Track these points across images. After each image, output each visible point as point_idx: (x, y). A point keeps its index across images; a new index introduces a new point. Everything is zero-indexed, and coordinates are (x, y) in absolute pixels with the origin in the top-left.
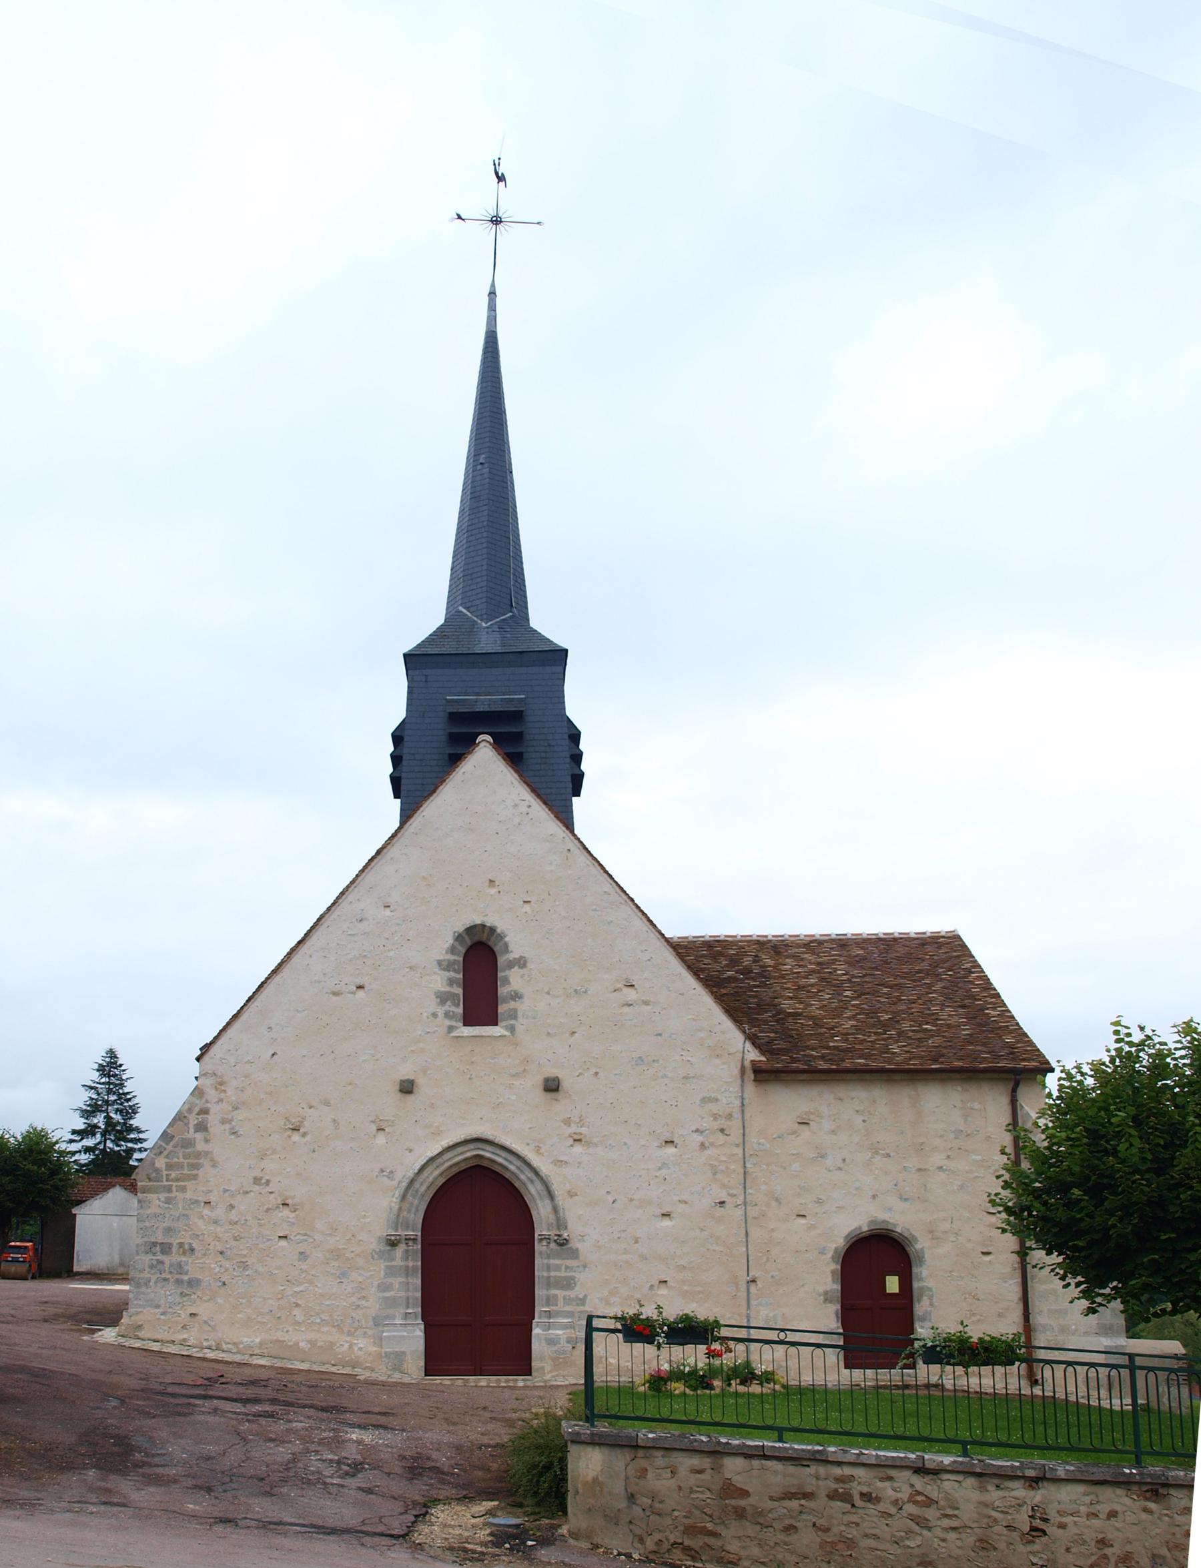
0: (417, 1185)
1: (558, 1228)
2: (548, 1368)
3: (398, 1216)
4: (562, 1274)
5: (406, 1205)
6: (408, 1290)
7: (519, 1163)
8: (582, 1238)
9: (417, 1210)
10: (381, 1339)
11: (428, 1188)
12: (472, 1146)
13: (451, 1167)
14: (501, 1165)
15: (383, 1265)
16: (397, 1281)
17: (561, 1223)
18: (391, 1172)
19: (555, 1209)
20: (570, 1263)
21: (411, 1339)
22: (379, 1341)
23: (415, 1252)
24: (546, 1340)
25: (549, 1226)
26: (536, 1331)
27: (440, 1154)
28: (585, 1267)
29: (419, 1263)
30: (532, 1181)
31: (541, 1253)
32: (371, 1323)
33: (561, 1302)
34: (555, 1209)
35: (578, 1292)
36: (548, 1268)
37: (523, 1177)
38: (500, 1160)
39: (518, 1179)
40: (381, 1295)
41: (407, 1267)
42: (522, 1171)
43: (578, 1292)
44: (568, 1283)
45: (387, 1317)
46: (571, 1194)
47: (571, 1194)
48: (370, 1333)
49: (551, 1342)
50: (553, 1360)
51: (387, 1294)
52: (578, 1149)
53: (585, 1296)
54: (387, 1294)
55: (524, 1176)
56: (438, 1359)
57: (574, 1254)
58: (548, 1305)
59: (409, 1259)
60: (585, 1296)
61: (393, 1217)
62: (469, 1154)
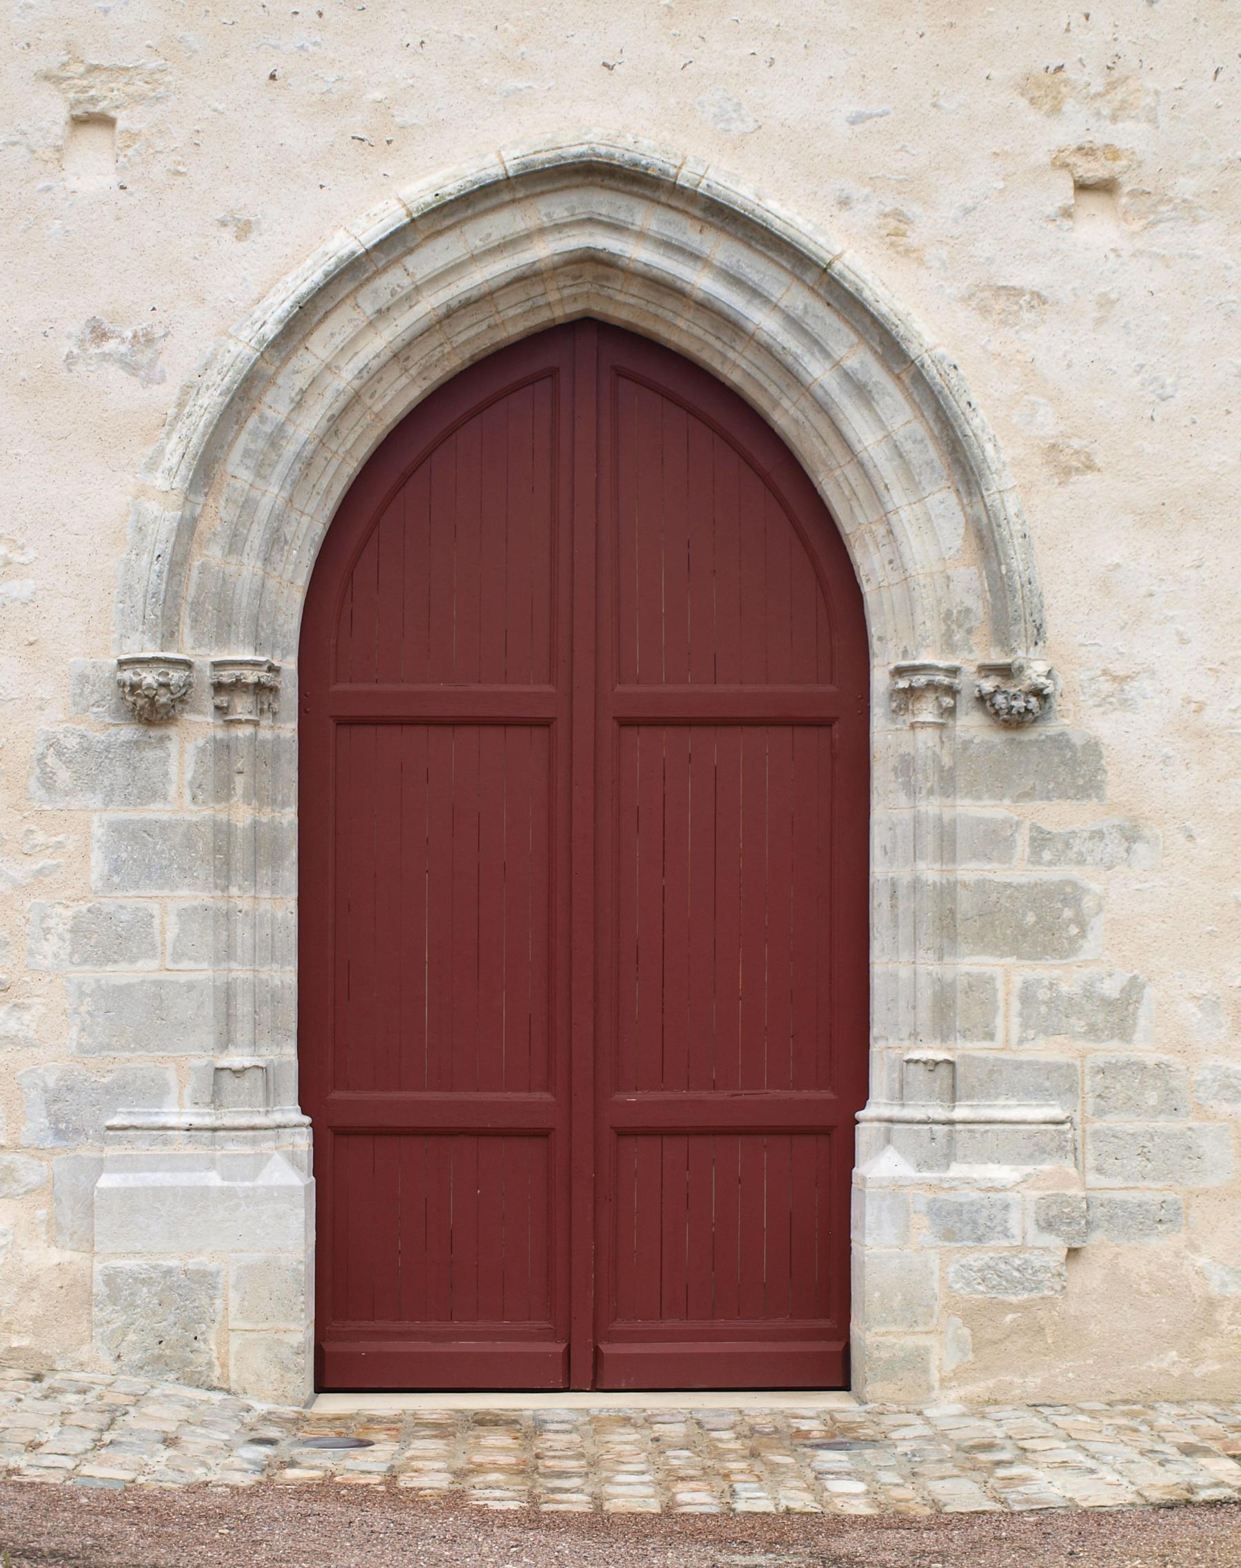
0: (275, 405)
1: (1002, 634)
2: (944, 1355)
3: (177, 565)
4: (1018, 871)
5: (218, 513)
6: (228, 953)
7: (796, 298)
8: (1119, 686)
9: (276, 541)
10: (88, 1205)
11: (335, 423)
12: (557, 207)
13: (450, 315)
14: (705, 307)
15: (96, 817)
16: (173, 905)
17: (1009, 606)
18: (146, 339)
19: (986, 539)
20: (1058, 815)
21: (258, 1203)
22: (79, 1215)
23: (263, 756)
24: (936, 1211)
25: (954, 622)
26: (879, 1166)
27: (396, 244)
28: (1131, 835)
29: (289, 816)
30: (862, 392)
31: (906, 766)
32: (36, 1124)
33: (1008, 1022)
34: (986, 539)
35: (1095, 965)
36: (947, 842)
37: (816, 370)
38: (702, 282)
39: (791, 376)
40: (88, 975)
41: (224, 832)
42: (815, 343)
43: (1095, 965)
44: (1045, 922)
45: (120, 1091)
46: (1065, 462)
47: (1065, 462)
48: (32, 1172)
49: (961, 1223)
50: (973, 1315)
51: (121, 974)
52: (1098, 228)
53: (1133, 989)
54: (121, 974)
55: (830, 361)
56: (379, 1311)
57: (1079, 770)
58: (943, 1029)
59: (235, 795)
60: (1133, 989)
61: (149, 571)
62: (543, 251)
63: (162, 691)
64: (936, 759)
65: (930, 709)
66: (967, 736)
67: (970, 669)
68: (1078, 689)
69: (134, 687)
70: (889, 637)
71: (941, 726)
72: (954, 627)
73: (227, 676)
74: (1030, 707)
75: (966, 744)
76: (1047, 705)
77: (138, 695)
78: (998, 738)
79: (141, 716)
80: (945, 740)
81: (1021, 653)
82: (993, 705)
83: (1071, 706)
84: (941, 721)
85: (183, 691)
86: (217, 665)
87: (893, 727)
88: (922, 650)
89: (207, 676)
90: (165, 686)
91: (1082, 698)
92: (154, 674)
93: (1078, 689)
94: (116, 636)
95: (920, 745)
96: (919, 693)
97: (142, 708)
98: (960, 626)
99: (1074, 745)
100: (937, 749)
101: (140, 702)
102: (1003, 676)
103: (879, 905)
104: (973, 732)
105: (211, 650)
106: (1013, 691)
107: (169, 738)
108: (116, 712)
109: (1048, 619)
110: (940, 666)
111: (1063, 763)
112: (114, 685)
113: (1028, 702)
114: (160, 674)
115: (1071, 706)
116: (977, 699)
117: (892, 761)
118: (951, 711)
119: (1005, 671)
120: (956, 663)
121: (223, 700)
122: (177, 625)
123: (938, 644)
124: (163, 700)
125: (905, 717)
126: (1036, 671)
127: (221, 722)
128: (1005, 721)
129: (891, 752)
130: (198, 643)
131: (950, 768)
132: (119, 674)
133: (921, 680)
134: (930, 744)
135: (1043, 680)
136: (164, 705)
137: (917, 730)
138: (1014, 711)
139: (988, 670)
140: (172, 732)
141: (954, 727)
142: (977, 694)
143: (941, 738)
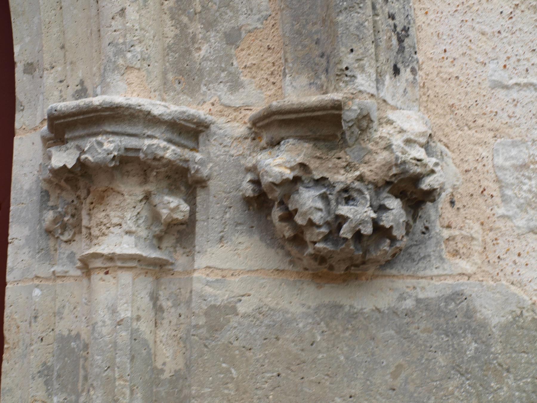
64: (141, 352)
65: (130, 225)
66: (220, 295)
67: (231, 127)
68: (492, 188)
70: (47, 59)
71: (158, 268)
72: (196, 28)
74: (387, 221)
75: (219, 316)
76: (419, 226)
78: (296, 301)
80: (166, 304)
81: (364, 82)
82: (289, 216)
83: (476, 230)
84: (154, 254)
87: (45, 270)
88: (115, 78)
91: (501, 211)
93: (492, 188)
95: (102, 315)
96: (101, 183)
98: (209, 25)
99: (484, 325)
100: (145, 327)
102: (316, 140)
104: (236, 285)
106: (342, 179)
109: (420, 19)
110: (157, 111)
111: (457, 368)
113: (382, 208)
115: (476, 230)
116: (248, 201)
117: (40, 354)
118: (181, 232)
119: (325, 126)
120: (201, 112)
123: (156, 68)
125: (74, 247)
126: (402, 125)
128: (321, 259)
129: (38, 328)
131: (178, 377)
133: (105, 146)
134: (125, 313)
135: (419, 153)
137: (96, 277)
138: (346, 232)
139: (273, 126)
141: (189, 271)
142: (248, 189)
143: (154, 298)
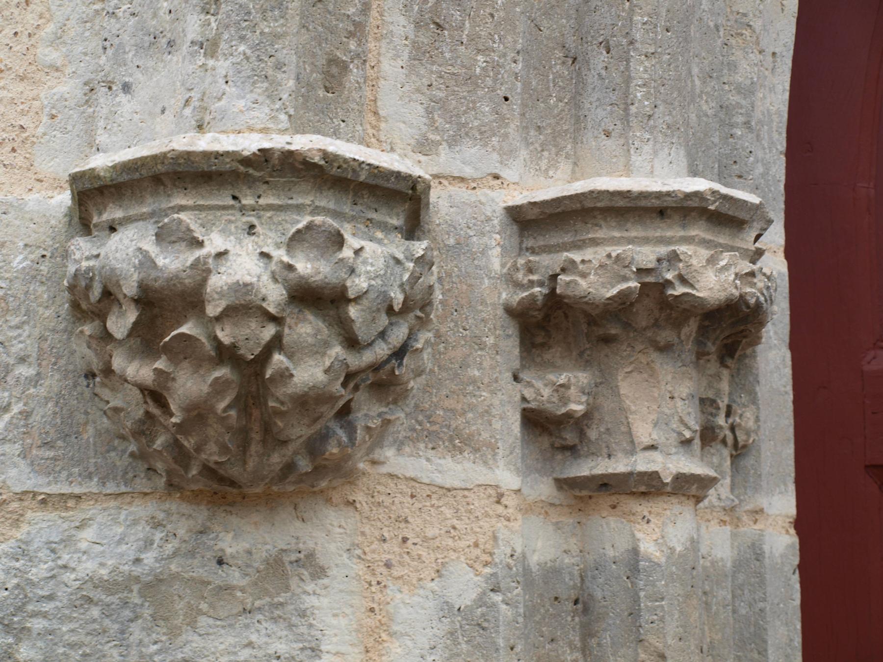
63: (306, 328)
69: (162, 307)
73: (597, 269)
77: (183, 349)
79: (181, 456)
85: (399, 334)
86: (530, 222)
89: (491, 274)
90: (319, 300)
92: (270, 240)
94: (67, 88)
97: (198, 414)
101: (189, 385)
103: (794, 573)
105: (507, 154)
107: (312, 565)
108: (56, 442)
112: (52, 310)
114: (296, 240)
121: (565, 385)
122: (358, 30)
124: (308, 374)
127: (545, 489)
130: (450, 121)
132: (82, 248)
136: (308, 402)
140: (330, 532)
